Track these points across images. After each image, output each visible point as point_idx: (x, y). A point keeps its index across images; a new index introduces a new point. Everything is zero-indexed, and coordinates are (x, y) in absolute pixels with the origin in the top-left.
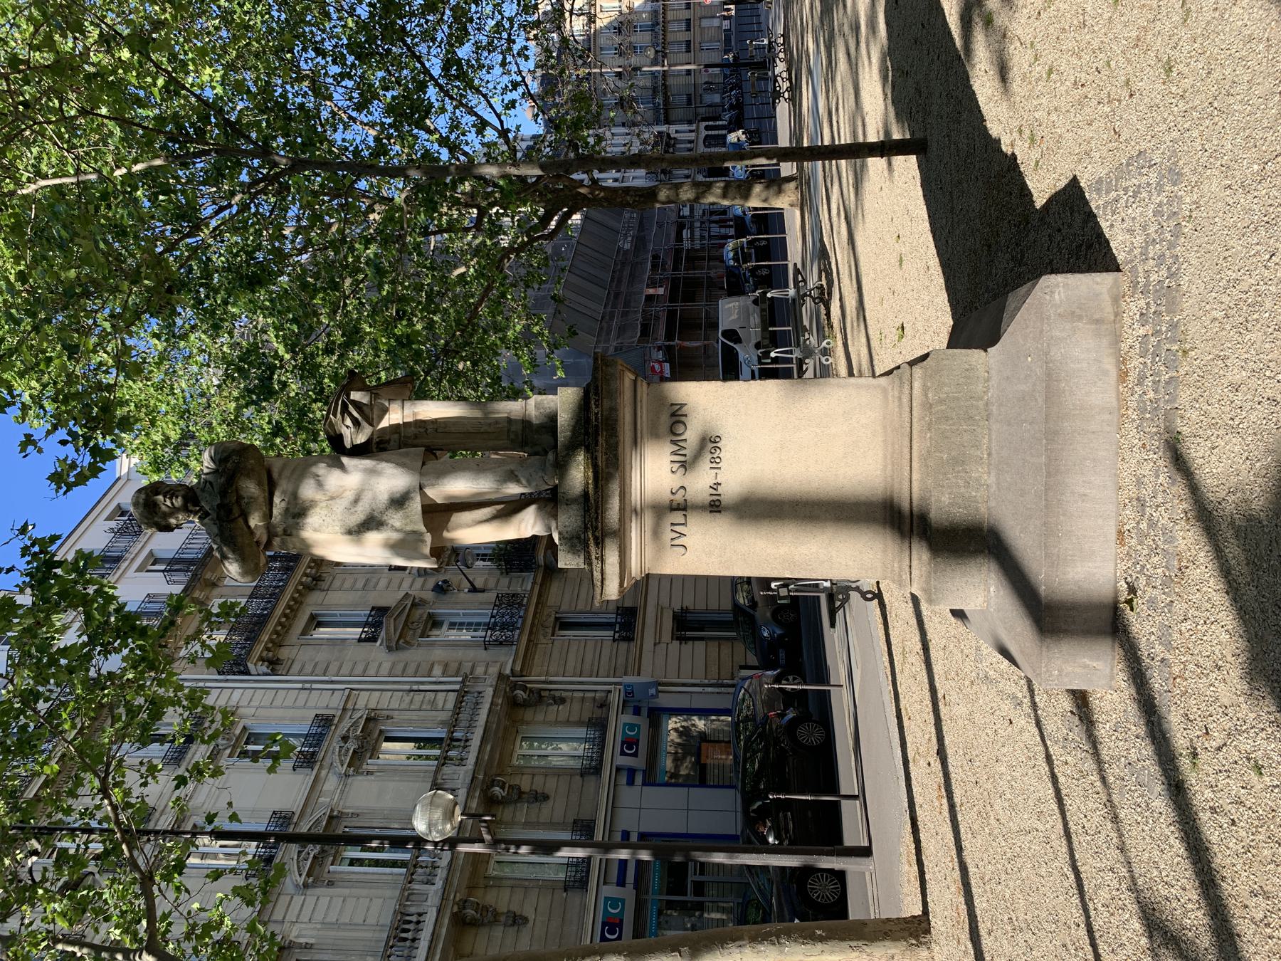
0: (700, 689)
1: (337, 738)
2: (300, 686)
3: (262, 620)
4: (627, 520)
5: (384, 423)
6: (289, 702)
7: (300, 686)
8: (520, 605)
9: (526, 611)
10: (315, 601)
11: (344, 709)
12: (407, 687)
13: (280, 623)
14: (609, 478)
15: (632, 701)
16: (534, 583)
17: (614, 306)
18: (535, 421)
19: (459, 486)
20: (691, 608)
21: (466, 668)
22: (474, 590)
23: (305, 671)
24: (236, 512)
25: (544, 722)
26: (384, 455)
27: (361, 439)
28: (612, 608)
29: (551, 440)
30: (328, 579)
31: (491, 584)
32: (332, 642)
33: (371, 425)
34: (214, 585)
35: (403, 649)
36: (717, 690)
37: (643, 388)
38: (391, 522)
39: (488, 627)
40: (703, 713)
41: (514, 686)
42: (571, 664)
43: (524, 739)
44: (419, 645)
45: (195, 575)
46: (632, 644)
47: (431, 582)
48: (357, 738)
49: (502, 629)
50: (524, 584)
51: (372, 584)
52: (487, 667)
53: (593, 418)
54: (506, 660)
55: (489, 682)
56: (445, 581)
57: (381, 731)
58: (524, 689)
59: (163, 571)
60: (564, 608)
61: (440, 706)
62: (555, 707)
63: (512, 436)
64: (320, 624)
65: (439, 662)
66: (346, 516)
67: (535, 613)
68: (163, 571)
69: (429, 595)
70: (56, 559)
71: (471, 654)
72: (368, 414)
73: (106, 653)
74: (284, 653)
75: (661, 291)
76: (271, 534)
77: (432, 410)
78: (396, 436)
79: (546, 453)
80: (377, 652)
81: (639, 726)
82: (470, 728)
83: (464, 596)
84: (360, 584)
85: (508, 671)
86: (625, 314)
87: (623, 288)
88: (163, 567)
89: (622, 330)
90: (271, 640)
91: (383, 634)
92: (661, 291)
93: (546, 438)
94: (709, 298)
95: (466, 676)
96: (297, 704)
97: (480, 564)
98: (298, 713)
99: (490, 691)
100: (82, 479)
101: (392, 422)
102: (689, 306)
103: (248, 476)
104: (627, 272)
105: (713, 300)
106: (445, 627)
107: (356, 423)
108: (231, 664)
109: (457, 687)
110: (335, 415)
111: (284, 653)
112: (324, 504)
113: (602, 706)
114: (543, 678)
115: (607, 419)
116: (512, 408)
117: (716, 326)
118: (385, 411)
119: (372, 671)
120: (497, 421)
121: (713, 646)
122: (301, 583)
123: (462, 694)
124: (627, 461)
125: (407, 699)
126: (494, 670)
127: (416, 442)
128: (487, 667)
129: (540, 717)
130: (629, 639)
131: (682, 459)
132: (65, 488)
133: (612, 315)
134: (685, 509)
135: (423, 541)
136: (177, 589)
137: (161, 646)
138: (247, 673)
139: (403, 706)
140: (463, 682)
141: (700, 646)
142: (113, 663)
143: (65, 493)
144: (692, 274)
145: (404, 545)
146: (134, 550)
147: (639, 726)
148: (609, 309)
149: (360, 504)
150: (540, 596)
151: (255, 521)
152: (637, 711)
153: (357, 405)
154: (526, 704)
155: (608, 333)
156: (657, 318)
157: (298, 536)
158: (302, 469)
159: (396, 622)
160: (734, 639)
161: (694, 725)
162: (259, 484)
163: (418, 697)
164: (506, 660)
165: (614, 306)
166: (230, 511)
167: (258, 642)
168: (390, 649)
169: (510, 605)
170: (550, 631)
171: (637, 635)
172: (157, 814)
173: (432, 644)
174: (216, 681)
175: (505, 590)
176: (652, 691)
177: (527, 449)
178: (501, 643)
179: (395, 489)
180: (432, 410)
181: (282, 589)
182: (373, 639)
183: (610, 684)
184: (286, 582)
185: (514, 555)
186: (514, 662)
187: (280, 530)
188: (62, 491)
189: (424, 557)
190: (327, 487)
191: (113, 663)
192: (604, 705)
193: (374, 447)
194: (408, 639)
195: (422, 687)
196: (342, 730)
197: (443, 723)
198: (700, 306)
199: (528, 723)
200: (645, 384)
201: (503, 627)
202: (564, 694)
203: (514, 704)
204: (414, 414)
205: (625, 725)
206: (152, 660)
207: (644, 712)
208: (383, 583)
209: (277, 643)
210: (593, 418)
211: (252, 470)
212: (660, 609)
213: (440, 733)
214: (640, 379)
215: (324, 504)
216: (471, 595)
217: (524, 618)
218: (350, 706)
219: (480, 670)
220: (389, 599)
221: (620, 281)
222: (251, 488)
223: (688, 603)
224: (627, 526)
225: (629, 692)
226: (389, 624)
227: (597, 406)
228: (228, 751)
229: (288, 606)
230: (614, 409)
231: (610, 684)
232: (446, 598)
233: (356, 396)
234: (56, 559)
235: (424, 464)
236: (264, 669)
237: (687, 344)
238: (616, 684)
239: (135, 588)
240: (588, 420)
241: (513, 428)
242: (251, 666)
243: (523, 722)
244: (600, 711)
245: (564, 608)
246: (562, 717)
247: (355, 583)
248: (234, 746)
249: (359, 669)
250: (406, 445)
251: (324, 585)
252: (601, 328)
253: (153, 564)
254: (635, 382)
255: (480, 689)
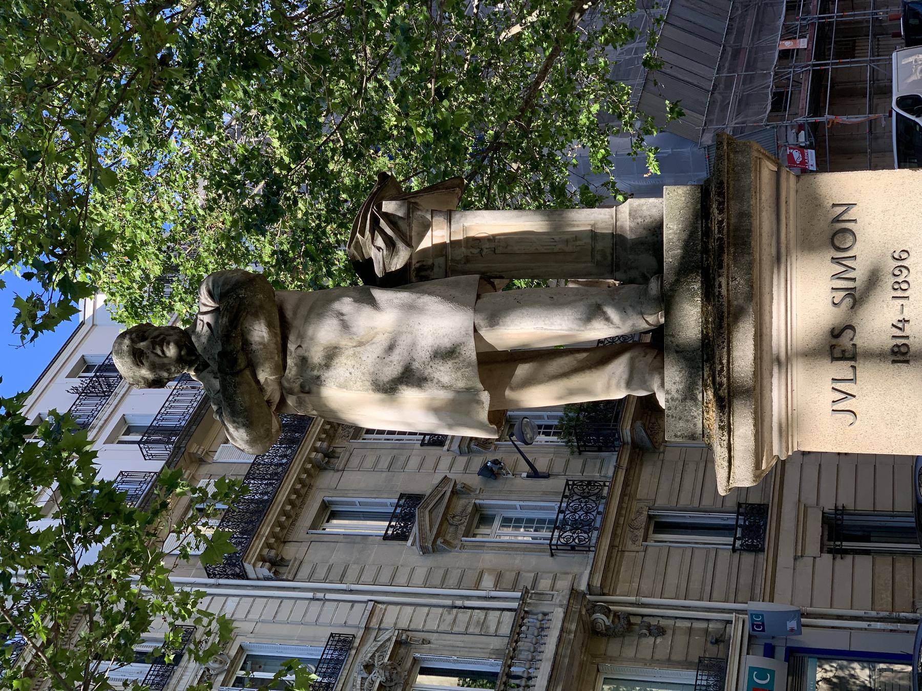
0: (864, 624)
1: (358, 666)
2: (310, 595)
3: (261, 508)
4: (766, 374)
5: (426, 243)
6: (297, 616)
7: (310, 595)
8: (599, 496)
9: (607, 505)
10: (328, 486)
11: (367, 628)
12: (449, 602)
13: (283, 512)
14: (737, 315)
15: (761, 635)
16: (617, 468)
17: (732, 70)
18: (629, 235)
19: (523, 329)
20: (850, 507)
21: (527, 580)
22: (535, 474)
23: (316, 576)
24: (242, 362)
25: (635, 660)
26: (427, 285)
27: (398, 263)
28: (731, 504)
29: (653, 261)
30: (344, 457)
31: (558, 467)
32: (351, 539)
33: (409, 244)
34: (201, 461)
35: (443, 551)
36: (890, 626)
37: (790, 182)
38: (436, 375)
39: (555, 525)
40: (868, 658)
41: (593, 608)
42: (672, 579)
43: (607, 681)
44: (463, 547)
45: (177, 448)
46: (761, 557)
47: (477, 462)
48: (384, 667)
49: (574, 530)
50: (604, 468)
51: (399, 464)
52: (555, 579)
53: (715, 228)
54: (581, 572)
55: (557, 600)
56: (496, 462)
57: (415, 660)
58: (607, 612)
59: (139, 443)
60: (659, 503)
61: (492, 630)
62: (652, 639)
63: (598, 257)
64: (334, 515)
65: (490, 571)
66: (381, 366)
67: (620, 508)
68: (139, 443)
69: (474, 480)
70: (28, 423)
71: (534, 561)
72: (403, 232)
73: (85, 542)
74: (290, 552)
75: (803, 43)
76: (285, 392)
77: (485, 223)
78: (441, 260)
79: (646, 280)
80: (407, 553)
81: (772, 673)
82: (533, 661)
83: (522, 482)
84: (384, 464)
85: (583, 587)
86: (748, 80)
87: (746, 42)
88: (138, 438)
89: (744, 103)
90: (273, 534)
91: (415, 529)
92: (803, 43)
93: (646, 260)
94: (876, 52)
95: (527, 592)
96: (307, 619)
97: (542, 438)
98: (310, 631)
99: (559, 613)
100: (49, 323)
101: (436, 241)
102: (845, 64)
103: (256, 316)
104: (750, 20)
105: (883, 54)
106: (497, 523)
107: (390, 244)
108: (226, 564)
109: (515, 605)
110: (363, 235)
111: (290, 552)
112: (351, 352)
113: (717, 642)
114: (632, 599)
115: (736, 229)
116: (586, 219)
117: (888, 91)
118: (426, 226)
119: (402, 578)
120: (577, 236)
121: (884, 565)
122: (309, 460)
123: (521, 615)
124: (766, 289)
125: (449, 618)
126: (564, 584)
127: (469, 266)
128: (555, 579)
129: (629, 652)
130: (757, 549)
131: (850, 284)
132: (32, 332)
133: (729, 82)
134: (853, 358)
135: (479, 402)
136: (157, 466)
137: (148, 534)
138: (244, 576)
139: (443, 628)
140: (522, 598)
141: (864, 562)
142: (89, 556)
143: (32, 339)
144: (850, 16)
145: (458, 407)
146: (103, 415)
147: (772, 673)
148: (724, 74)
149: (397, 351)
150: (626, 484)
151: (265, 375)
152: (769, 652)
153: (391, 219)
154: (608, 634)
155: (724, 108)
156: (797, 83)
157: (318, 394)
158: (320, 302)
159: (432, 517)
160: (915, 553)
161: (853, 676)
162: (270, 326)
163: (464, 616)
164: (581, 572)
165: (732, 70)
166: (235, 362)
167: (256, 535)
168: (425, 550)
169: (585, 497)
170: (641, 533)
171: (769, 543)
172: (357, 641)
173: (481, 546)
174: (206, 585)
175: (578, 476)
176: (792, 624)
177: (617, 274)
178: (573, 548)
179: (441, 332)
180: (485, 223)
181: (286, 468)
182: (402, 536)
183: (730, 611)
184: (291, 459)
185: (590, 426)
186: (591, 574)
187: (296, 386)
188: (28, 337)
189: (480, 426)
190: (354, 329)
191: (89, 556)
192: (720, 640)
193: (413, 274)
194: (448, 538)
195: (468, 603)
196: (366, 654)
197: (497, 653)
198: (862, 63)
199: (612, 659)
200: (792, 179)
201: (577, 526)
202: (663, 622)
203: (593, 632)
204: (465, 229)
205: (752, 669)
206: (136, 553)
207: (781, 652)
208: (414, 463)
209: (281, 538)
210: (715, 228)
211: (261, 307)
212: (803, 510)
213: (493, 666)
214: (784, 170)
215: (351, 352)
216: (530, 482)
217: (605, 515)
218: (374, 624)
219: (544, 584)
220: (423, 484)
221: (740, 33)
222: (260, 332)
223: (846, 500)
224: (765, 382)
225: (758, 625)
226: (423, 517)
227: (721, 211)
228: (221, 678)
229: (294, 491)
230: (745, 215)
231: (732, 612)
232: (498, 484)
233: (389, 206)
234: (28, 423)
235: (478, 297)
236: (265, 571)
237: (843, 119)
238: (738, 611)
239: (118, 462)
240: (707, 233)
241: (599, 246)
242: (249, 568)
243: (606, 657)
244: (714, 649)
245: (659, 503)
246: (661, 654)
247: (378, 461)
248: (228, 671)
249: (385, 576)
250: (455, 272)
251: (339, 463)
252: (713, 103)
253: (127, 433)
254: (778, 174)
255: (546, 610)
